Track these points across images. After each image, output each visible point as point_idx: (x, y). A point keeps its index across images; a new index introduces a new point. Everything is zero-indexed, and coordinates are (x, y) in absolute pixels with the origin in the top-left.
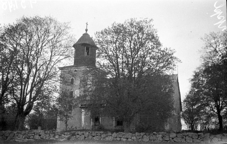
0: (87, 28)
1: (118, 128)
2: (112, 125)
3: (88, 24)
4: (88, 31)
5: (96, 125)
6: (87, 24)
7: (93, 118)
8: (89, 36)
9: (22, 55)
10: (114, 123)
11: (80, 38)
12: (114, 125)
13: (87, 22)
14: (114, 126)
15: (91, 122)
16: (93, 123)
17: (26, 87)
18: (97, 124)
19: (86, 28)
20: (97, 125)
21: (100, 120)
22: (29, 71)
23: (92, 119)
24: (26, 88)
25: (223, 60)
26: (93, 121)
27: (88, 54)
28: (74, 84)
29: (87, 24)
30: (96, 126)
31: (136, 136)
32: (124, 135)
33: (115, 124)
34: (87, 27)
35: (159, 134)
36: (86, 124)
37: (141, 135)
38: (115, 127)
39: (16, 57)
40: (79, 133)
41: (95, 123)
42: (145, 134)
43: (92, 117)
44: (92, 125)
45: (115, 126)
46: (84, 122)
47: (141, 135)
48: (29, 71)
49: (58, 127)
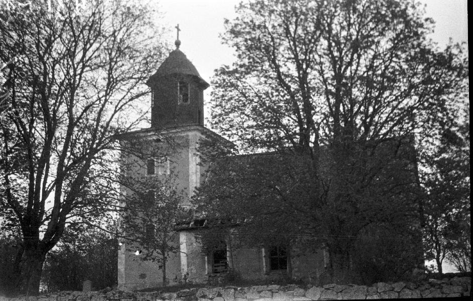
0: (180, 39)
1: (276, 275)
2: (260, 270)
3: (180, 28)
4: (180, 46)
5: (217, 273)
6: (179, 30)
7: (208, 255)
8: (185, 56)
9: (424, 161)
10: (264, 264)
11: (194, 66)
12: (265, 269)
13: (178, 25)
14: (265, 272)
15: (205, 264)
16: (211, 267)
17: (43, 176)
18: (220, 269)
19: (176, 38)
20: (219, 272)
21: (228, 259)
22: (50, 133)
23: (206, 258)
24: (42, 180)
25: (181, 89)
26: (208, 263)
27: (186, 100)
28: (155, 173)
29: (179, 30)
30: (218, 275)
31: (380, 293)
32: (341, 292)
33: (266, 266)
34: (179, 37)
35: (451, 284)
36: (193, 271)
37: (394, 288)
38: (267, 274)
39: (295, 140)
40: (207, 293)
41: (215, 267)
42: (404, 285)
43: (206, 251)
44: (208, 273)
45: (266, 271)
46: (188, 267)
47: (396, 290)
48: (50, 133)
49: (121, 283)
